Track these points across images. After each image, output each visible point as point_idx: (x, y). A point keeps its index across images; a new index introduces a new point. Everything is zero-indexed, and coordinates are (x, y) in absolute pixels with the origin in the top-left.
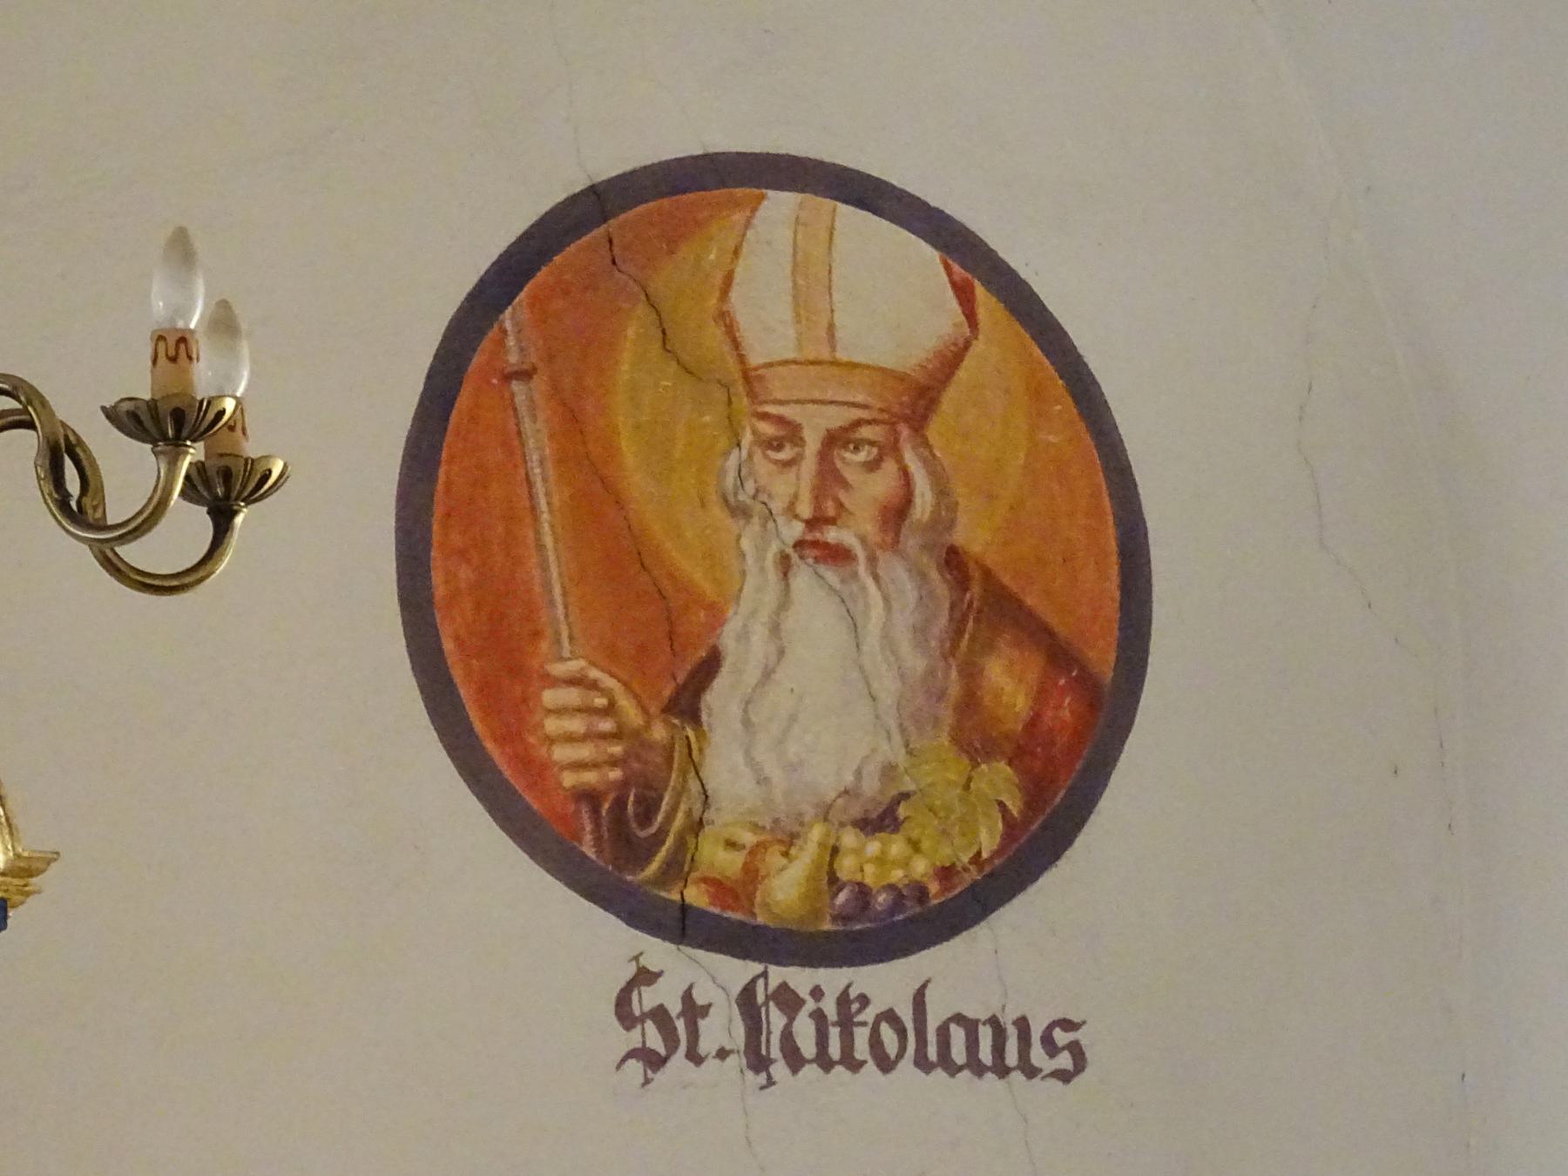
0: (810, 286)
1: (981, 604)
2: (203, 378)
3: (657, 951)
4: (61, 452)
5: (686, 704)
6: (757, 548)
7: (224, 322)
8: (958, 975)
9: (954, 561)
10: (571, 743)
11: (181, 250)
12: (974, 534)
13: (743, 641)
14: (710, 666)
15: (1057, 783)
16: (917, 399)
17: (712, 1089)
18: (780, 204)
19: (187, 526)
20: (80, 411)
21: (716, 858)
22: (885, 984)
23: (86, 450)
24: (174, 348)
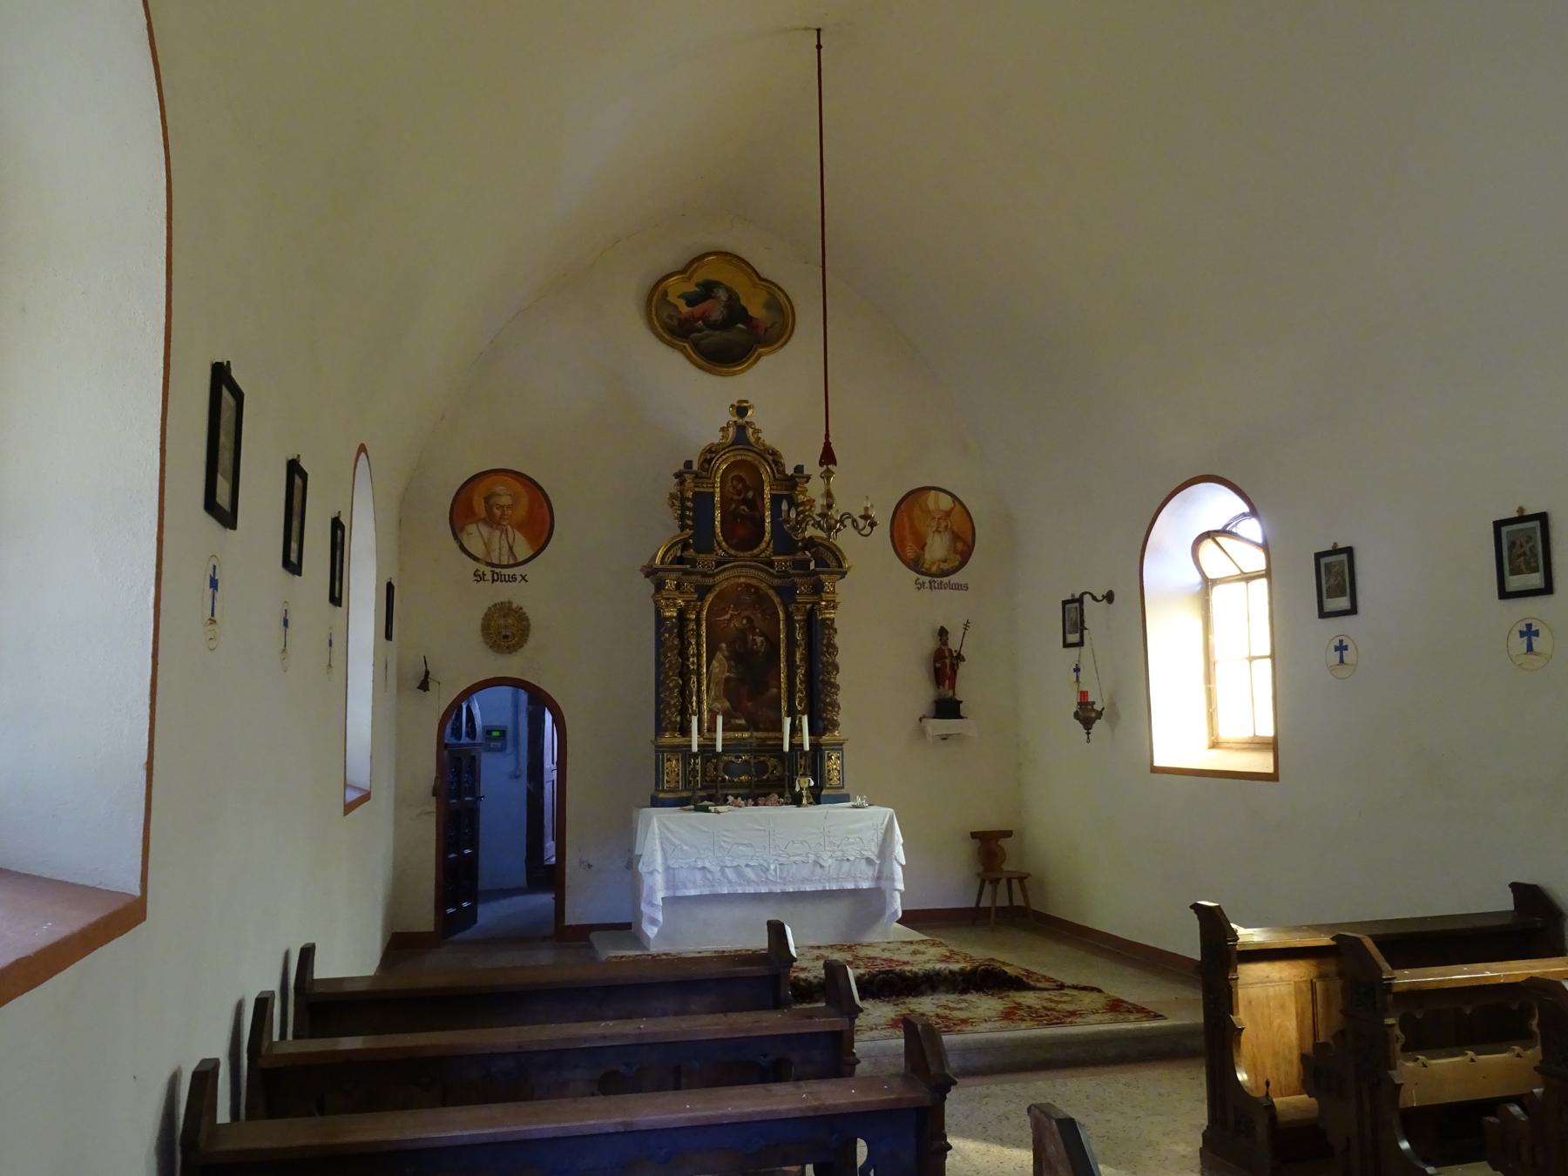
0: (936, 502)
1: (956, 537)
4: (854, 521)
8: (954, 579)
10: (910, 553)
12: (955, 528)
13: (929, 541)
15: (964, 561)
16: (948, 514)
17: (926, 591)
20: (856, 517)
22: (945, 580)
24: (866, 509)
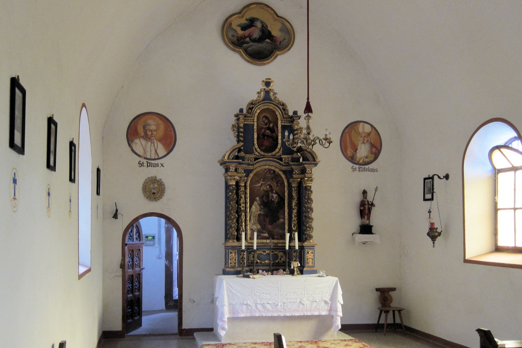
1: (372, 146)
2: (328, 137)
3: (354, 165)
5: (356, 151)
6: (360, 143)
7: (330, 133)
8: (371, 166)
9: (371, 143)
10: (349, 152)
11: (326, 129)
12: (372, 142)
13: (359, 148)
14: (357, 149)
15: (376, 158)
16: (369, 134)
17: (357, 173)
18: (362, 123)
19: (327, 145)
21: (357, 160)
22: (367, 167)
23: (315, 154)
24: (326, 135)
